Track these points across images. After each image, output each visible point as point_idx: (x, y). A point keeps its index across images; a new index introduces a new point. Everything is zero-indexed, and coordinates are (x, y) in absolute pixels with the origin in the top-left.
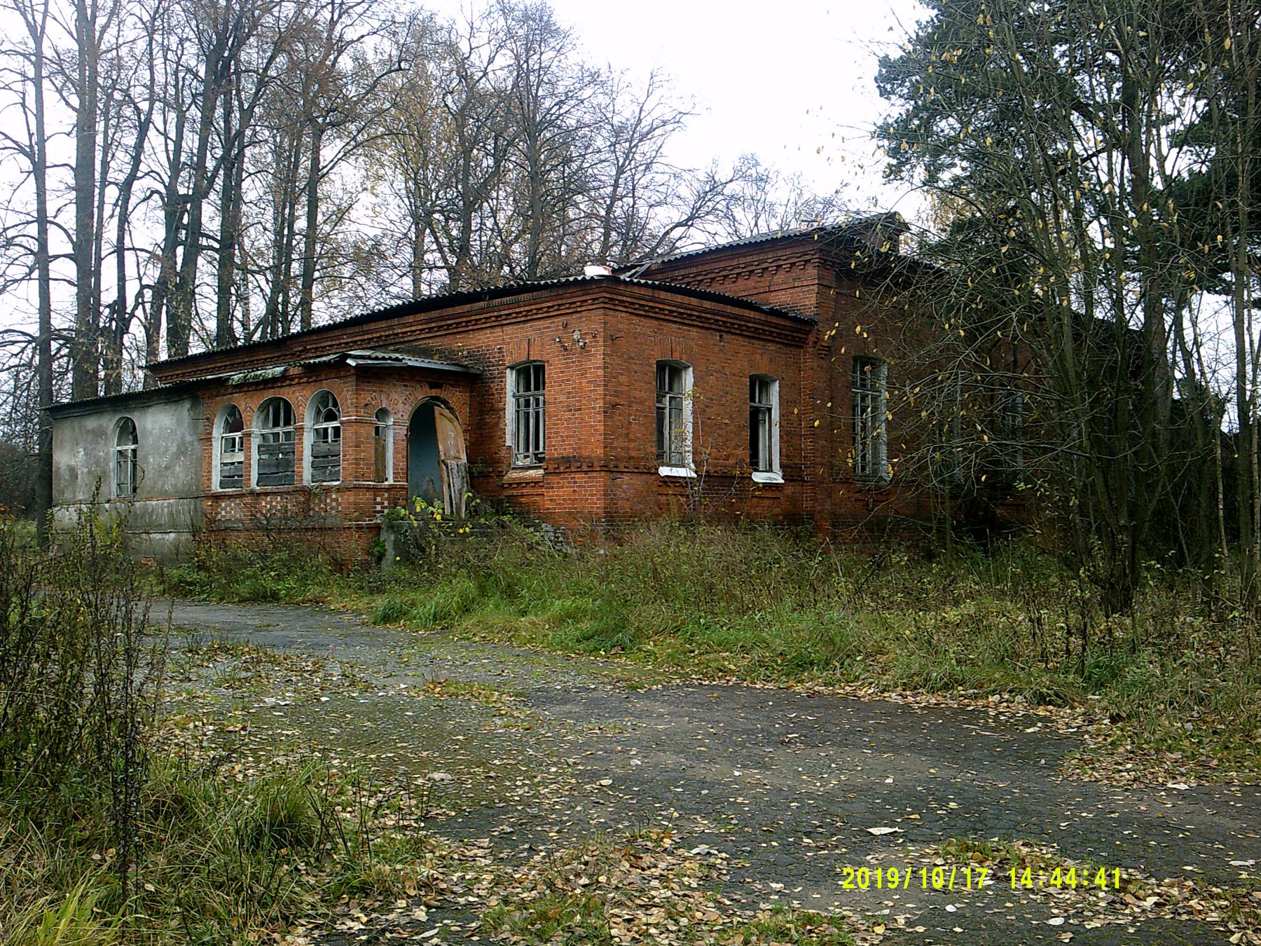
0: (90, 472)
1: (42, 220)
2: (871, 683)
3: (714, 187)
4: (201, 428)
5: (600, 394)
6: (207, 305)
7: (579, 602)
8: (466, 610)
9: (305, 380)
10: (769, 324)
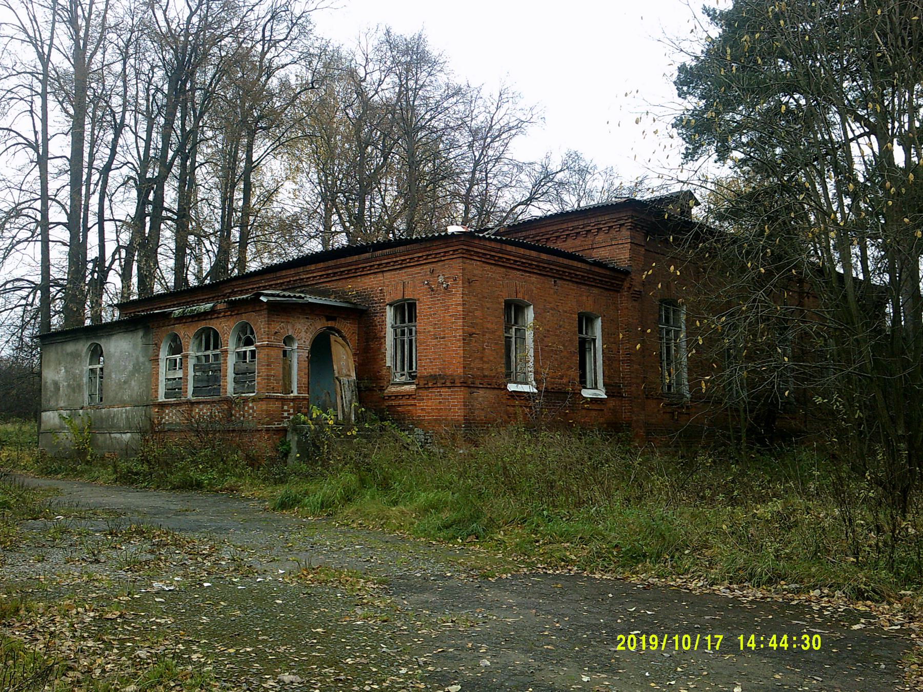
0: (69, 386)
1: (45, 197)
2: (701, 576)
3: (547, 176)
4: (151, 351)
5: (460, 326)
6: (166, 263)
7: (441, 495)
8: (348, 499)
9: (229, 313)
10: (593, 273)
